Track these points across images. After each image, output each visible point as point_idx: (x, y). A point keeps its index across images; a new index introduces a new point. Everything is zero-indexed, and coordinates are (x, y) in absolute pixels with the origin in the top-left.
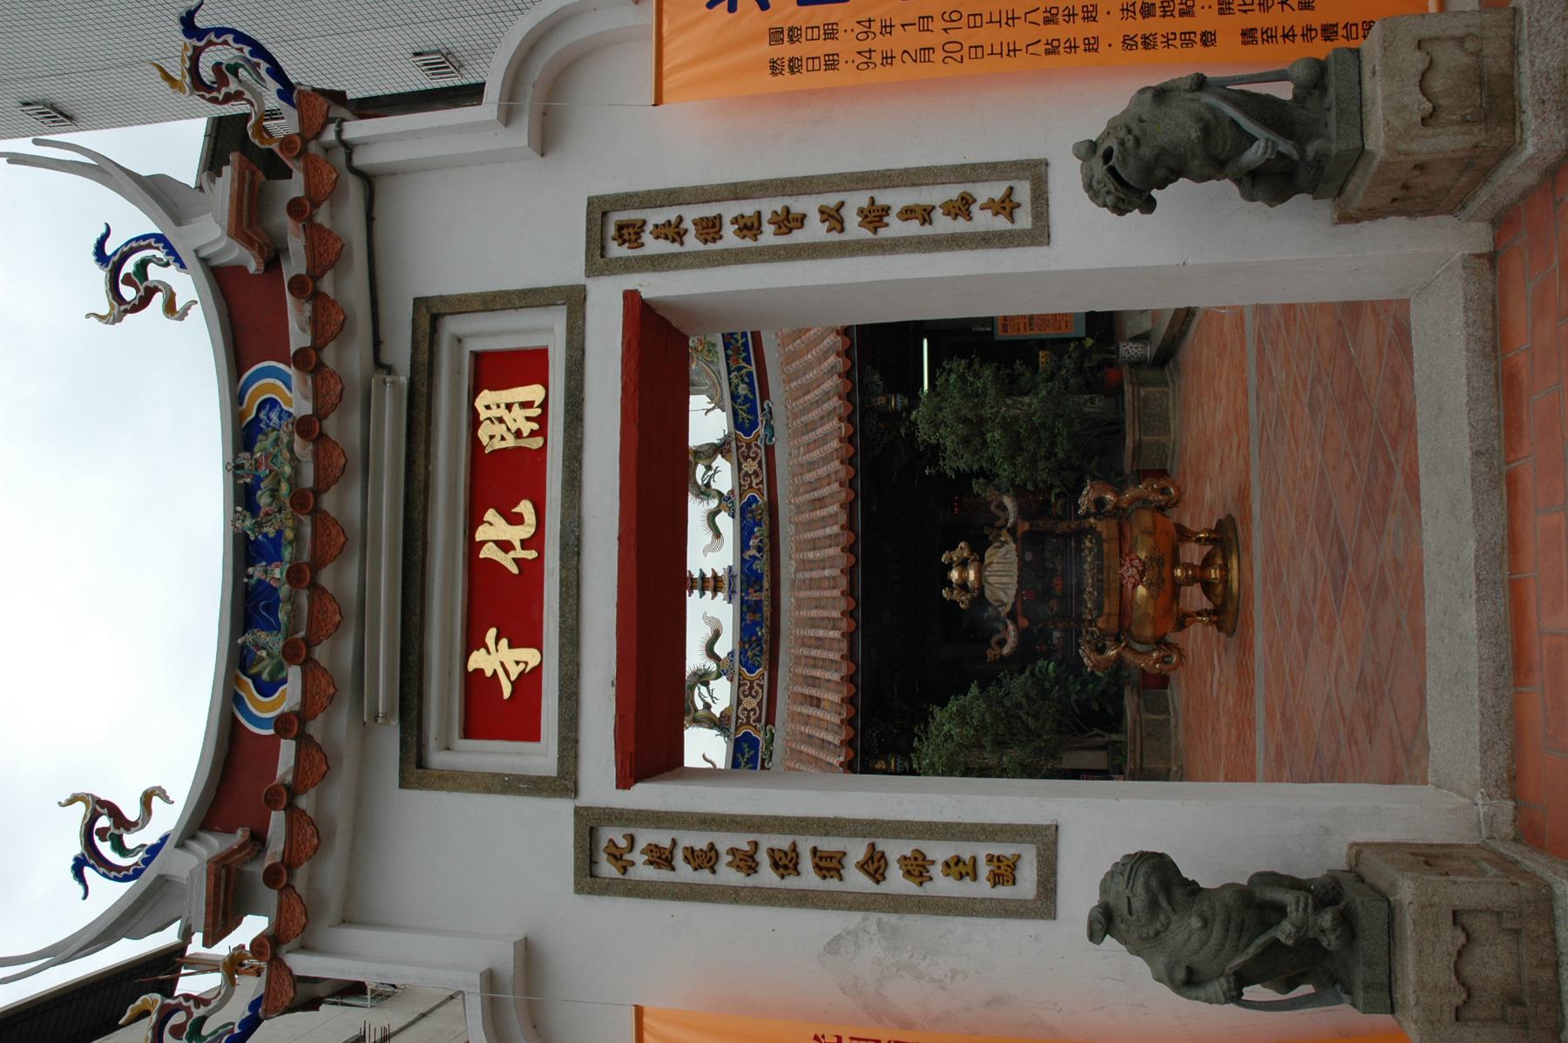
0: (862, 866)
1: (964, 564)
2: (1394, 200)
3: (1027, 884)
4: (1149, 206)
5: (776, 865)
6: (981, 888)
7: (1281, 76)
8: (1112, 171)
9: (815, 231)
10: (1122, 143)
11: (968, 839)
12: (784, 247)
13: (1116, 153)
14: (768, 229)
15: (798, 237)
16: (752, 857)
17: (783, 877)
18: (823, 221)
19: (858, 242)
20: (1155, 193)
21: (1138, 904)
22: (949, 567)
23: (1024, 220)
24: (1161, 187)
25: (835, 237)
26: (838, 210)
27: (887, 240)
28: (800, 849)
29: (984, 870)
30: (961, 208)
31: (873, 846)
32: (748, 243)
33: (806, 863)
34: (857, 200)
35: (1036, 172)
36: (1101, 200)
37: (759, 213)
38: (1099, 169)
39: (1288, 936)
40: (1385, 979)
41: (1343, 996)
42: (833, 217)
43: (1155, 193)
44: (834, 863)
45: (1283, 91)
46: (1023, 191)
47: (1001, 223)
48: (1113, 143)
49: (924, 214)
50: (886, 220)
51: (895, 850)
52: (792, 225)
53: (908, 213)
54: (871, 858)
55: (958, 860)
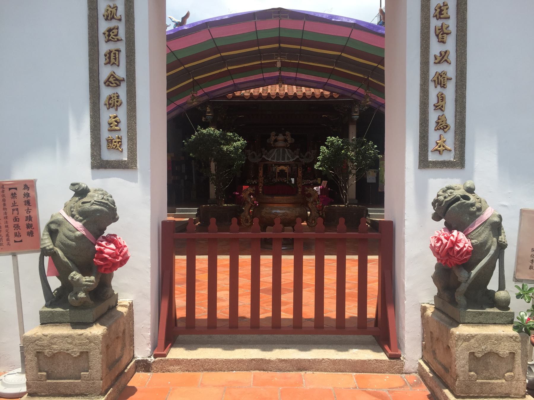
0: (112, 75)
1: (286, 141)
2: (431, 333)
3: (108, 155)
4: (436, 217)
5: (110, 30)
6: (105, 134)
7: (502, 287)
8: (457, 199)
9: (435, 48)
10: (473, 205)
11: (128, 127)
12: (428, 32)
13: (467, 202)
14: (439, 23)
15: (433, 40)
16: (113, 18)
17: (104, 34)
18: (440, 53)
19: (428, 71)
20: (443, 221)
21: (87, 206)
22: (284, 135)
23: (432, 157)
24: (446, 224)
25: (432, 60)
26: (446, 60)
27: (428, 86)
28: (119, 43)
29: (115, 135)
30: (442, 126)
31: (123, 80)
32: (432, 12)
33: (112, 46)
34: (450, 70)
35: (460, 162)
36: (441, 193)
37: (449, 18)
38: (458, 193)
39: (73, 278)
40: (56, 321)
41: (50, 302)
42: (443, 58)
43: (443, 221)
44: (113, 61)
45: (493, 285)
46: (449, 157)
47: (432, 145)
48: (472, 199)
49: (439, 107)
50: (439, 87)
51: (122, 91)
52: (440, 36)
53: (441, 98)
54: (117, 80)
55: (118, 122)
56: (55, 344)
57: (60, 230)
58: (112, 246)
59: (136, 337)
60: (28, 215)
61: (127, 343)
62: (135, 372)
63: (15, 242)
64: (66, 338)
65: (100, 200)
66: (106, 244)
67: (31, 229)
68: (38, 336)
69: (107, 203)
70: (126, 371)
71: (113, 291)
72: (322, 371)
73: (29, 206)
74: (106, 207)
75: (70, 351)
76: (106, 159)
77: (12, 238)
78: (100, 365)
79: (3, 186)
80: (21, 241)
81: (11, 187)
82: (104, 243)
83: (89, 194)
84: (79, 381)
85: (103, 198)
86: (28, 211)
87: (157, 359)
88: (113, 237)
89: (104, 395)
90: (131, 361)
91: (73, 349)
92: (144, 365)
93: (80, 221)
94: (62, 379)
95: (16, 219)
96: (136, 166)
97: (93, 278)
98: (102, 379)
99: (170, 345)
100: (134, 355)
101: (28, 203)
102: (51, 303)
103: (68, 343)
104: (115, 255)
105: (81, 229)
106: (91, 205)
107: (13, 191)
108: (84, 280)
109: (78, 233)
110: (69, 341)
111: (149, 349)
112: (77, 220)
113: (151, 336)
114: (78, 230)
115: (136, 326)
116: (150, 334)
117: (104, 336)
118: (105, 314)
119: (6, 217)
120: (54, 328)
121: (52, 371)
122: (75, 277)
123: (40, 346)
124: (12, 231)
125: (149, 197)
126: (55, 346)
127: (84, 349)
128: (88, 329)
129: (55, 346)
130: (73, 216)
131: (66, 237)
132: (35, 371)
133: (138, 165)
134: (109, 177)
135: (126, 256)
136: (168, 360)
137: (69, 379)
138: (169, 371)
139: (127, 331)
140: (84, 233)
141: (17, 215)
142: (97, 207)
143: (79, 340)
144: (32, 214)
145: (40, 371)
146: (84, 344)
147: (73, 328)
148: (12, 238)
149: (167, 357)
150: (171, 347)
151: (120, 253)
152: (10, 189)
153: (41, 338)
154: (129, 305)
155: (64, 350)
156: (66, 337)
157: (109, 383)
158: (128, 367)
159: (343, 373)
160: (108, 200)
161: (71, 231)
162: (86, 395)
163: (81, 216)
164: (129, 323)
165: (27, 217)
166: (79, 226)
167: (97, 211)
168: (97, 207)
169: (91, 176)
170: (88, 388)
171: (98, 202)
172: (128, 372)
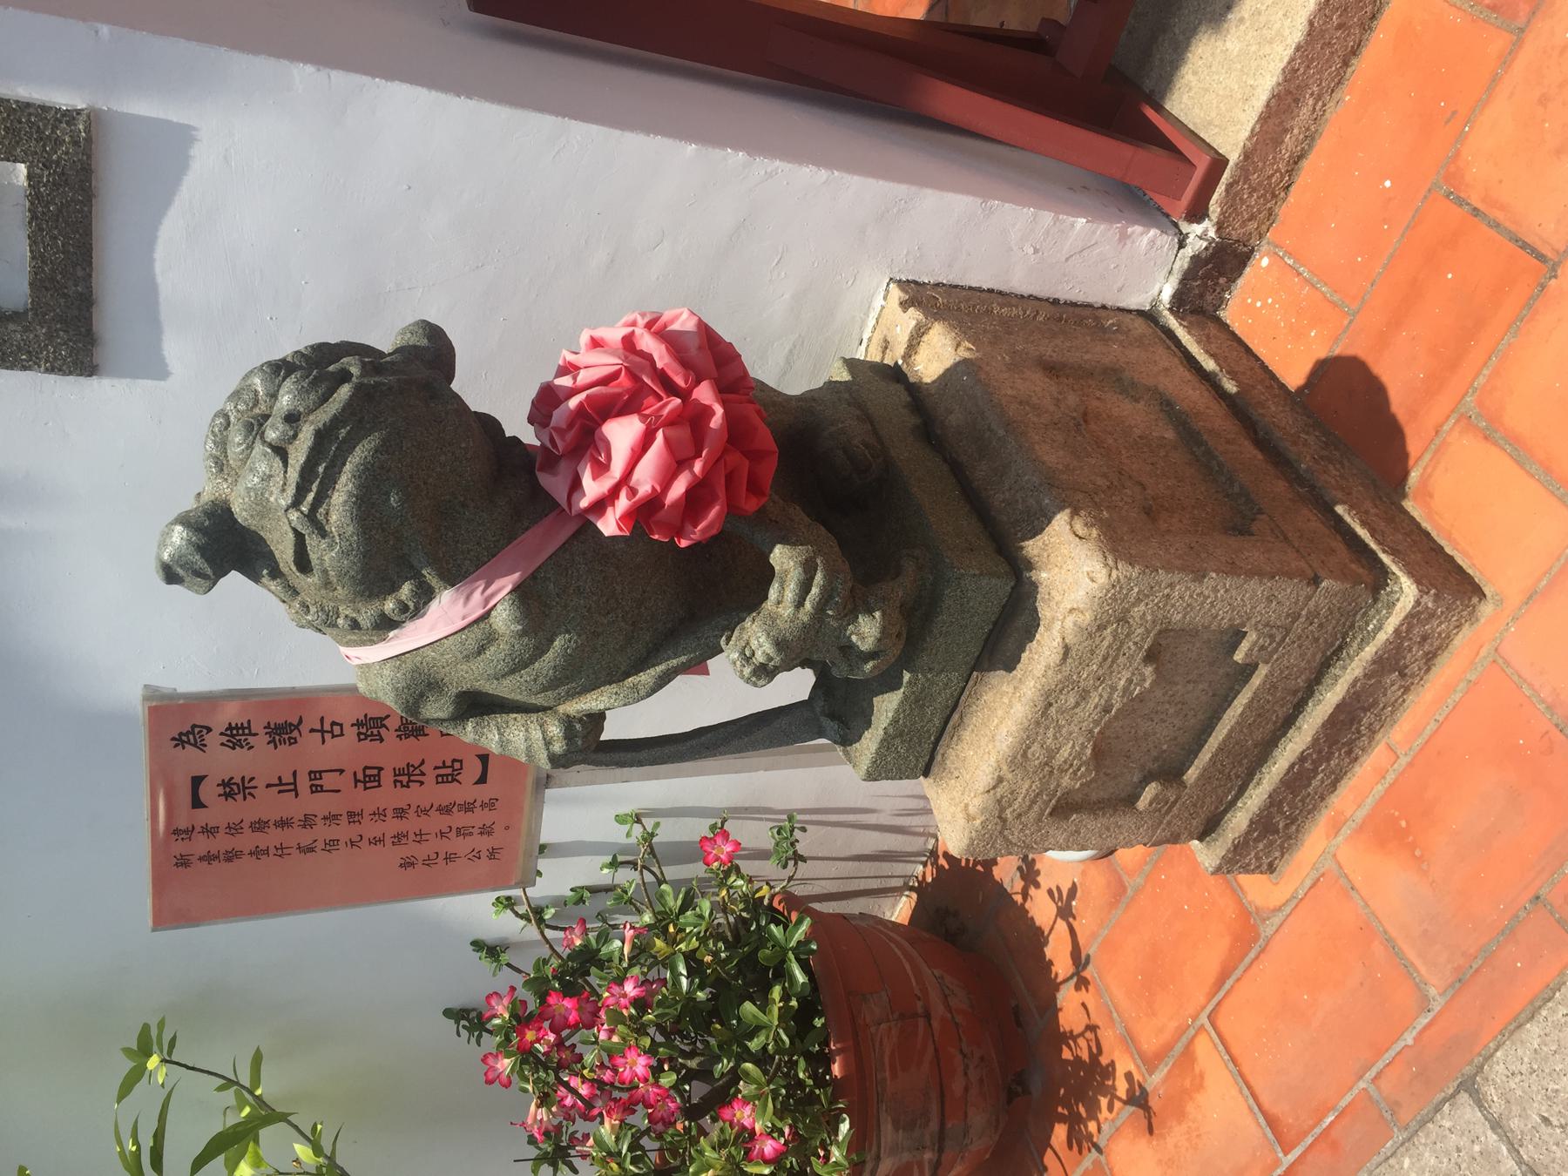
58: (622, 433)
59: (1066, 292)
60: (351, 733)
61: (1098, 354)
62: (1224, 327)
63: (482, 779)
65: (293, 475)
66: (601, 469)
68: (983, 811)
69: (322, 436)
70: (1230, 387)
71: (831, 386)
73: (304, 728)
74: (347, 448)
76: (26, 289)
78: (1253, 583)
79: (176, 832)
82: (592, 488)
83: (241, 510)
85: (281, 452)
86: (329, 730)
87: (1214, 207)
88: (559, 417)
89: (1384, 572)
90: (1170, 334)
91: (1113, 688)
92: (1207, 276)
93: (425, 595)
95: (369, 778)
96: (70, 116)
97: (782, 557)
98: (1315, 581)
99: (1150, 113)
100: (1140, 313)
101: (282, 733)
102: (832, 716)
103: (1077, 704)
104: (682, 433)
105: (477, 596)
106: (323, 533)
107: (208, 792)
108: (786, 611)
109: (504, 618)
110: (1072, 701)
111: (1147, 239)
112: (414, 610)
113: (1094, 216)
114: (486, 616)
115: (1020, 281)
116: (1081, 221)
117: (1115, 543)
118: (957, 470)
119: (351, 814)
120: (966, 735)
121: (1156, 759)
122: (760, 658)
123: (1030, 807)
125: (303, 74)
126: (1065, 753)
127: (1135, 648)
128: (1044, 612)
129: (1065, 753)
130: (385, 625)
131: (512, 672)
132: (1127, 821)
133: (64, 98)
134: (152, 289)
135: (693, 345)
136: (1247, 155)
137: (1227, 702)
138: (1301, 157)
139: (1049, 349)
140: (505, 585)
141: (348, 775)
142: (340, 498)
143: (1083, 663)
144: (347, 716)
145: (1132, 799)
146: (1119, 643)
147: (1010, 665)
148: (466, 790)
149: (1234, 157)
150: (1159, 108)
151: (671, 389)
152: (197, 803)
154: (913, 316)
155: (1097, 723)
156: (1044, 714)
157: (1310, 520)
158: (1209, 365)
160: (292, 419)
161: (481, 650)
163: (394, 588)
164: (1006, 323)
166: (459, 608)
167: (366, 506)
168: (340, 498)
170: (1316, 640)
171: (301, 491)
172: (1233, 375)
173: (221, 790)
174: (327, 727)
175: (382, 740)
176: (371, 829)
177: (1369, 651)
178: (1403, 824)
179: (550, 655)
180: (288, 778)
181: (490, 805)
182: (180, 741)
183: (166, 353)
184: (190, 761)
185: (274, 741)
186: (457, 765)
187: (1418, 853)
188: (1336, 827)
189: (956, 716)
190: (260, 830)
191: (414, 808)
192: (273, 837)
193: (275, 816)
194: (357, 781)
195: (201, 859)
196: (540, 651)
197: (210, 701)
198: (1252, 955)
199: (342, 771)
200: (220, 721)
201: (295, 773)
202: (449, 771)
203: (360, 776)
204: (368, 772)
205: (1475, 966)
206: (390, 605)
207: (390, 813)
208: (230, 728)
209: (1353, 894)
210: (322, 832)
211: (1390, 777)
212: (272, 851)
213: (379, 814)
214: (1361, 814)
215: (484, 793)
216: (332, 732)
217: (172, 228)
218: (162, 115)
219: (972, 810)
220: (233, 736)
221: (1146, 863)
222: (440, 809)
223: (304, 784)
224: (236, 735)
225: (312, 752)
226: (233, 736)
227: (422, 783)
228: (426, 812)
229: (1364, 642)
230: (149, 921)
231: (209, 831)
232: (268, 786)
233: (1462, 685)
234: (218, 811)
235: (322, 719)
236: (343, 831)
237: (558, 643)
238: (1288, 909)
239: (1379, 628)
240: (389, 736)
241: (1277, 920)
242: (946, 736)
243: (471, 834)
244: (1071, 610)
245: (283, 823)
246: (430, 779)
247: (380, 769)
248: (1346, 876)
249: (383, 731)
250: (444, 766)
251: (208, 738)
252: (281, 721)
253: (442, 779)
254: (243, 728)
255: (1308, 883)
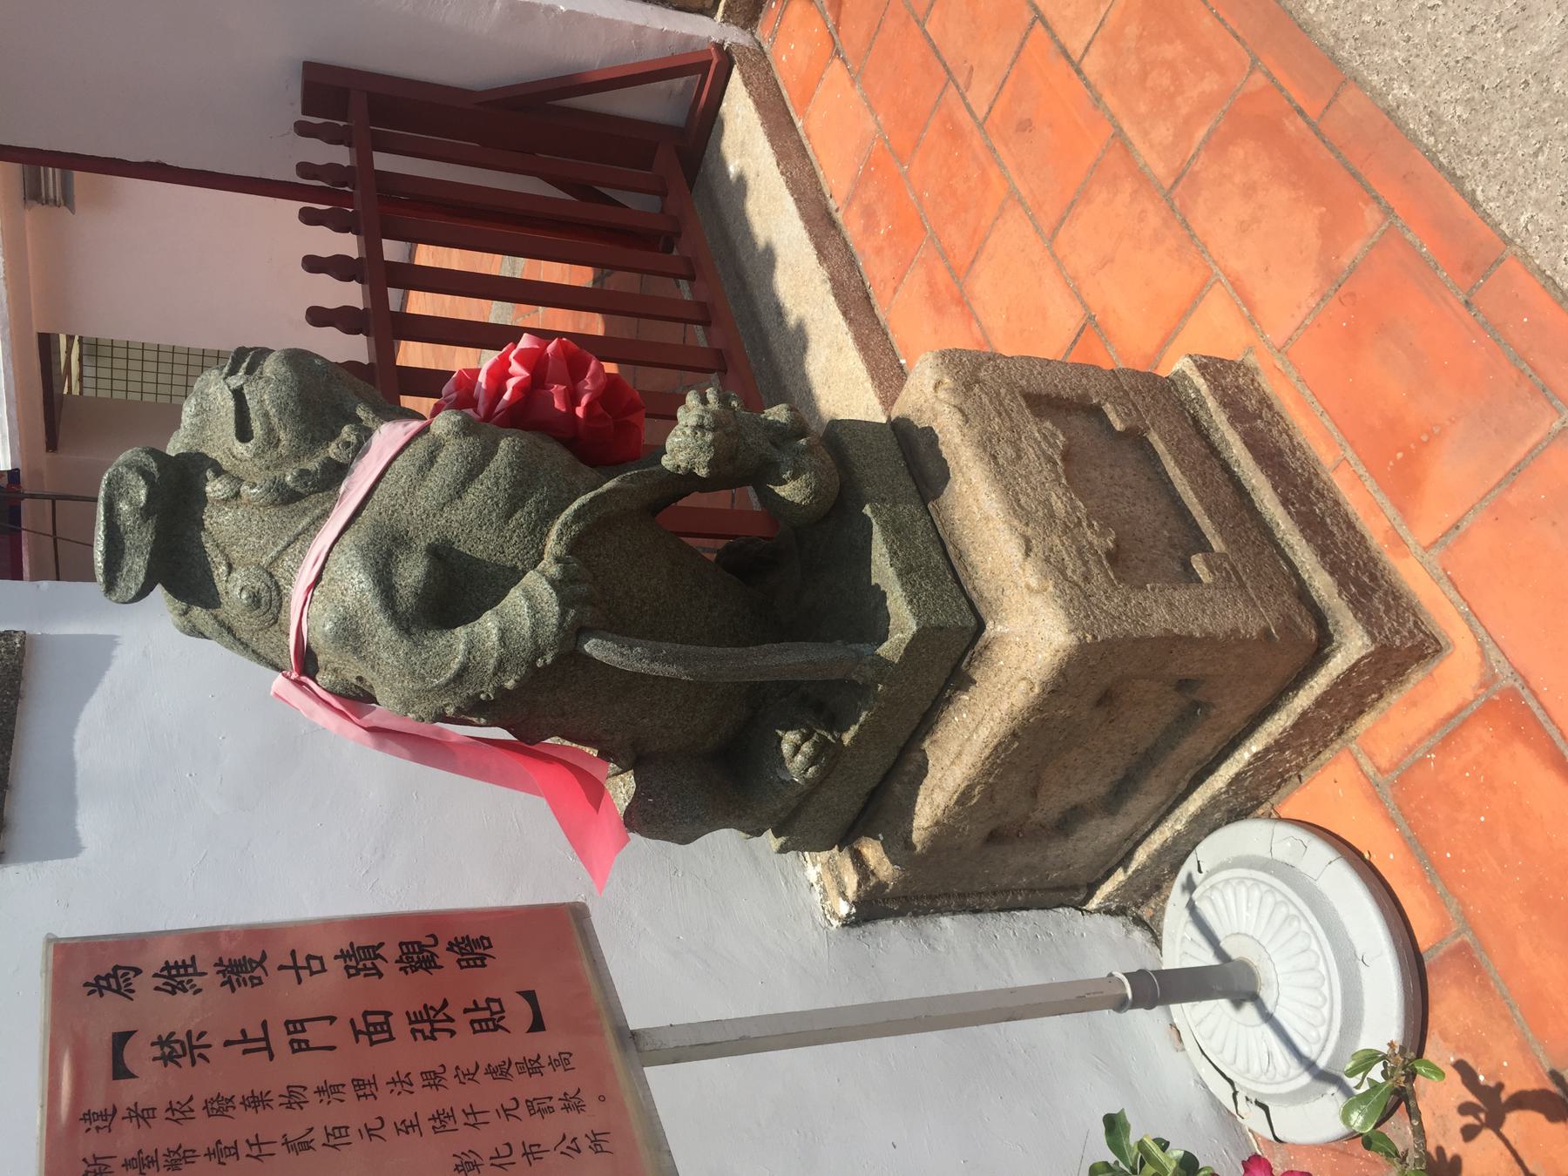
56: (1046, 503)
57: (432, 535)
60: (336, 968)
64: (1001, 461)
67: (441, 950)
72: (818, 182)
75: (1050, 451)
77: (515, 1043)
79: (88, 1117)
80: (530, 996)
81: (101, 1062)
84: (1154, 438)
86: (303, 965)
93: (366, 434)
94: (1183, 512)
95: (374, 1028)
103: (1019, 457)
110: (1010, 452)
112: (359, 449)
119: (358, 1084)
120: (974, 557)
123: (1085, 563)
124: (463, 1048)
126: (1059, 506)
127: (1018, 406)
130: (336, 473)
134: (70, 764)
137: (1167, 484)
144: (328, 949)
147: (944, 475)
148: (515, 1043)
152: (120, 1071)
153: (1047, 560)
156: (997, 464)
159: (806, 142)
161: (432, 459)
162: (1196, 421)
163: (334, 435)
165: (351, 972)
169: (52, 868)
173: (157, 1051)
174: (301, 962)
175: (380, 975)
176: (397, 1107)
177: (1211, 403)
178: (1400, 455)
179: (500, 453)
180: (255, 1032)
181: (563, 1061)
182: (98, 986)
183: (79, 828)
184: (110, 1013)
185: (229, 981)
186: (495, 1007)
187: (1424, 438)
188: (1398, 541)
189: (950, 548)
190: (221, 1112)
191: (451, 1072)
192: (240, 1126)
193: (241, 1090)
194: (357, 1033)
195: (127, 1164)
196: (488, 453)
197: (141, 941)
198: (1532, 704)
199: (332, 1019)
200: (152, 962)
201: (264, 1025)
202: (487, 1014)
203: (361, 1026)
204: (371, 1019)
205: (1529, 371)
206: (333, 450)
207: (417, 1080)
208: (167, 967)
209: (1464, 525)
210: (318, 1115)
211: (1362, 471)
212: (243, 1149)
213: (401, 1082)
214: (1391, 511)
215: (547, 1045)
216: (309, 967)
217: (94, 712)
218: (89, 632)
219: (1034, 583)
220: (171, 977)
221: (1433, 887)
222: (490, 1071)
223: (280, 1039)
224: (176, 977)
225: (288, 997)
226: (171, 977)
227: (453, 1033)
228: (471, 1076)
229: (1203, 405)
230: (64, 933)
231: (141, 1115)
232: (227, 1043)
233: (1299, 385)
234: (152, 1082)
235: (293, 953)
236: (351, 1112)
237: (503, 444)
238: (1481, 630)
239: (1198, 391)
240: (390, 969)
241: (1494, 655)
242: (960, 571)
243: (551, 1110)
244: (936, 387)
245: (257, 1101)
246: (462, 1024)
247: (387, 1014)
248: (1445, 534)
249: (378, 962)
250: (477, 1008)
251: (136, 982)
252: (238, 957)
253: (479, 1026)
254: (185, 966)
255: (1453, 594)
